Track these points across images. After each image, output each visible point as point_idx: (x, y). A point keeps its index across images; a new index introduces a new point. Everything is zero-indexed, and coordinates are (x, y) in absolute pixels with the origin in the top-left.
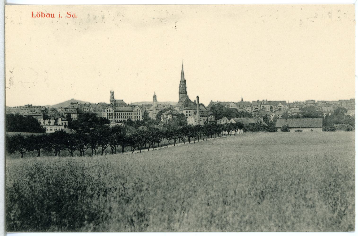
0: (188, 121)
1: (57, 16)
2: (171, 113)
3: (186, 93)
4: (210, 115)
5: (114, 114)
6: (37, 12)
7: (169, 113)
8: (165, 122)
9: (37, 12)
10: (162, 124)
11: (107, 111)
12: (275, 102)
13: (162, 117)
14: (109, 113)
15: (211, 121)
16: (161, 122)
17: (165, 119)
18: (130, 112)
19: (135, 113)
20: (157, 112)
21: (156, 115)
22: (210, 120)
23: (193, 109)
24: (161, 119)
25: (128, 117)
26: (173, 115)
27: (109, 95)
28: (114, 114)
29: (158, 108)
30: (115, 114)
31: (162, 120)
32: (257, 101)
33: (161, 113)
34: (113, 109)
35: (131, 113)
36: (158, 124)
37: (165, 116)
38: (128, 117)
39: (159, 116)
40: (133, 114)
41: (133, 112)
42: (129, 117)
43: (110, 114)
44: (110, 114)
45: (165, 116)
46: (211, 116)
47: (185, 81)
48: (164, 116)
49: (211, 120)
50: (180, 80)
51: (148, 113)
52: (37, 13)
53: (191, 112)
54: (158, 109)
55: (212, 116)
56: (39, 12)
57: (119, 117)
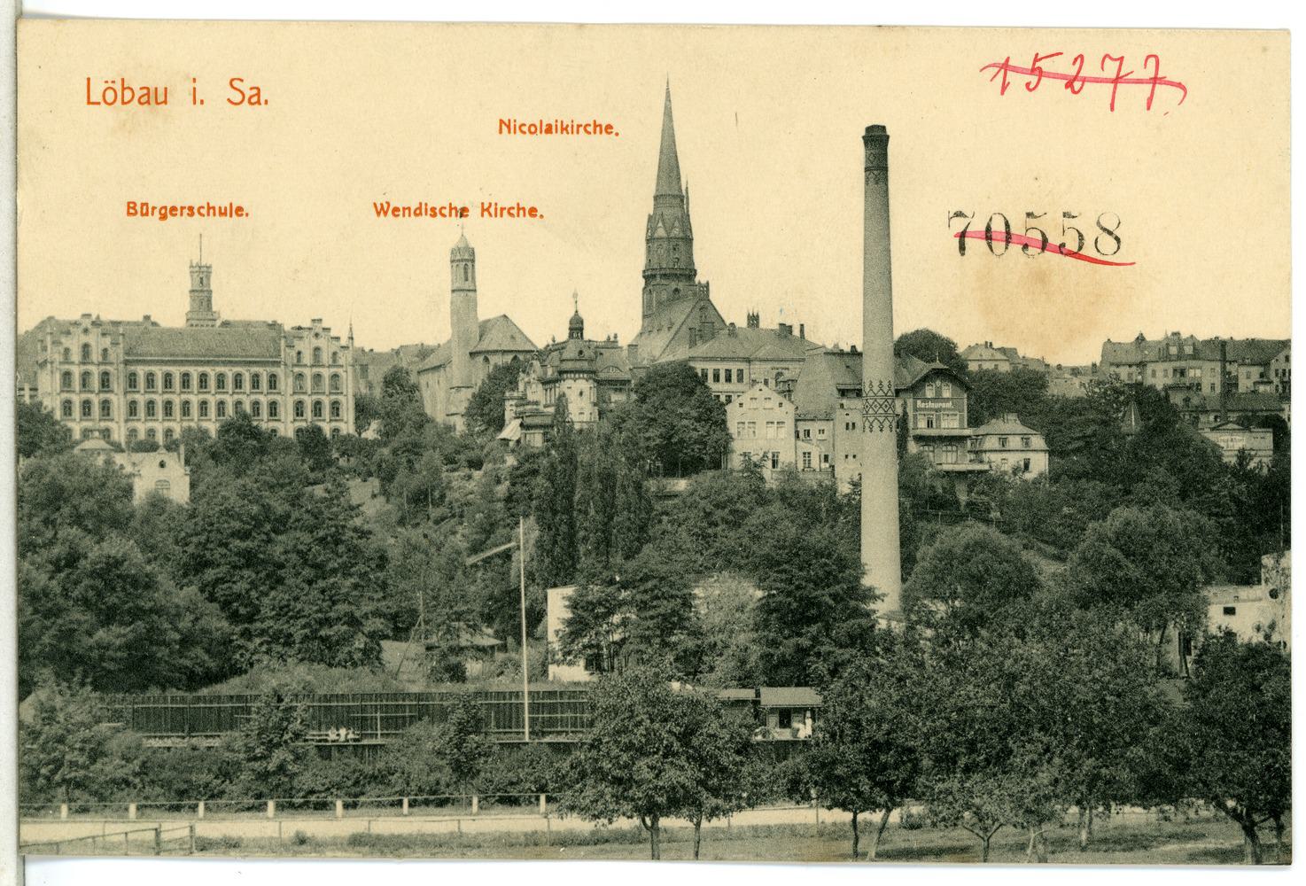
0: (732, 427)
1: (180, 95)
2: (585, 365)
3: (690, 274)
4: (926, 379)
5: (118, 384)
6: (106, 82)
7: (568, 366)
8: (537, 440)
9: (106, 82)
10: (511, 461)
11: (58, 358)
12: (1252, 344)
13: (510, 409)
14: (76, 371)
15: (933, 432)
16: (506, 441)
17: (537, 421)
18: (255, 369)
19: (300, 376)
20: (480, 374)
21: (467, 394)
22: (922, 424)
23: (761, 354)
24: (500, 424)
25: (221, 404)
26: (599, 383)
27: (186, 283)
28: (118, 384)
29: (483, 346)
30: (132, 381)
31: (512, 431)
32: (1133, 339)
33: (507, 376)
34: (115, 344)
35: (264, 373)
36: (476, 464)
37: (536, 393)
38: (221, 404)
39: (487, 410)
40: (286, 383)
41: (280, 371)
42: (230, 410)
43: (85, 376)
44: (85, 376)
45: (536, 393)
46: (929, 392)
47: (681, 199)
48: (531, 397)
49: (930, 424)
50: (650, 189)
51: (415, 388)
52: (107, 85)
53: (740, 379)
54: (486, 355)
55: (939, 391)
56: (113, 82)
57: (168, 407)
